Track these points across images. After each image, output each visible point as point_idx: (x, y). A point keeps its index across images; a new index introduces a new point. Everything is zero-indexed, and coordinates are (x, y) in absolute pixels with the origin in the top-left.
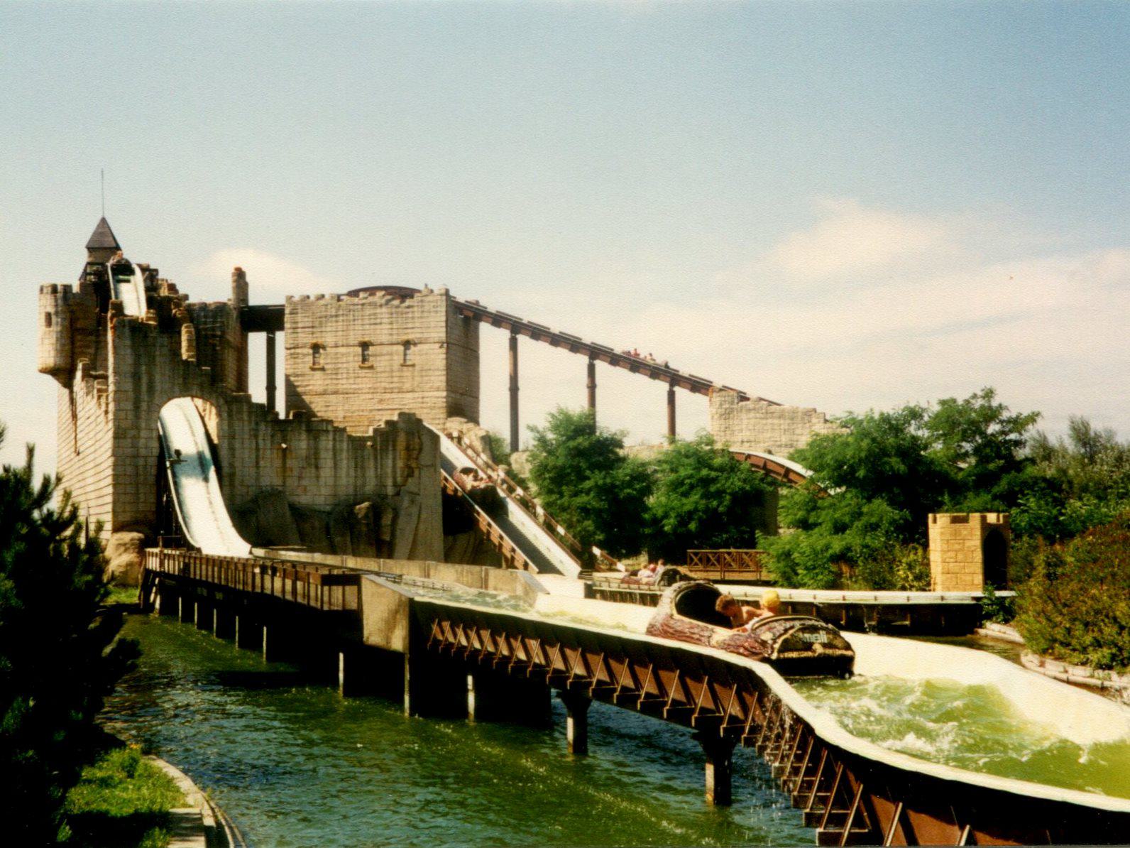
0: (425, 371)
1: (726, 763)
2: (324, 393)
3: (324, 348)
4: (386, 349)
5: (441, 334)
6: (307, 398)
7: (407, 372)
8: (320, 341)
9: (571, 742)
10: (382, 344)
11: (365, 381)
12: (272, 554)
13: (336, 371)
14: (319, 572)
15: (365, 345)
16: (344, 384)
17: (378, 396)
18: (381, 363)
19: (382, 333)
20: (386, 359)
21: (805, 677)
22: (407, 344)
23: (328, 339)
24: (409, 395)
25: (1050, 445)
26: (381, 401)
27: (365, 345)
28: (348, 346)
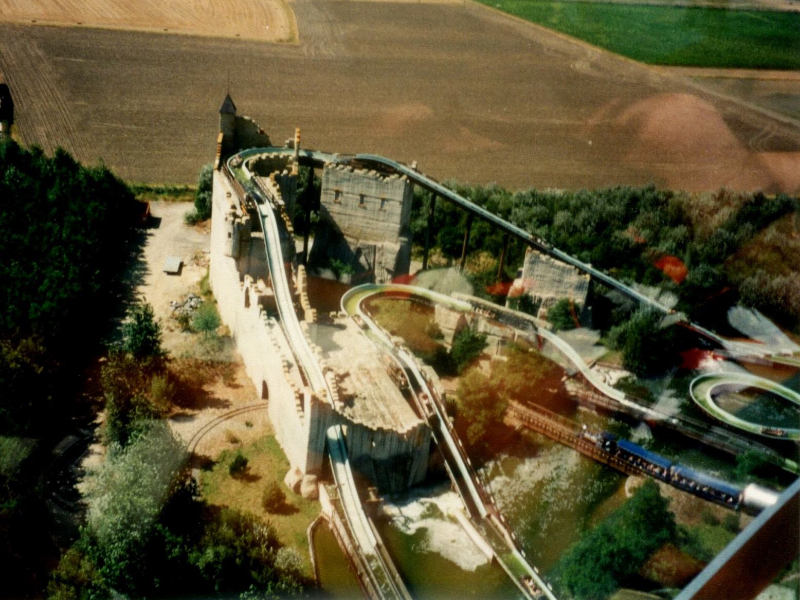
0: (391, 214)
1: (654, 340)
2: (339, 213)
3: (342, 193)
4: (373, 200)
5: (401, 198)
6: (331, 214)
7: (382, 213)
8: (340, 189)
9: (431, 427)
10: (371, 197)
11: (360, 213)
12: (467, 379)
13: (346, 205)
14: (54, 142)
15: (362, 196)
16: (349, 211)
17: (366, 220)
18: (369, 206)
19: (373, 192)
20: (373, 204)
21: (695, 438)
22: (383, 200)
23: (345, 189)
24: (381, 224)
25: (305, 575)
26: (368, 223)
27: (362, 196)
28: (353, 194)
